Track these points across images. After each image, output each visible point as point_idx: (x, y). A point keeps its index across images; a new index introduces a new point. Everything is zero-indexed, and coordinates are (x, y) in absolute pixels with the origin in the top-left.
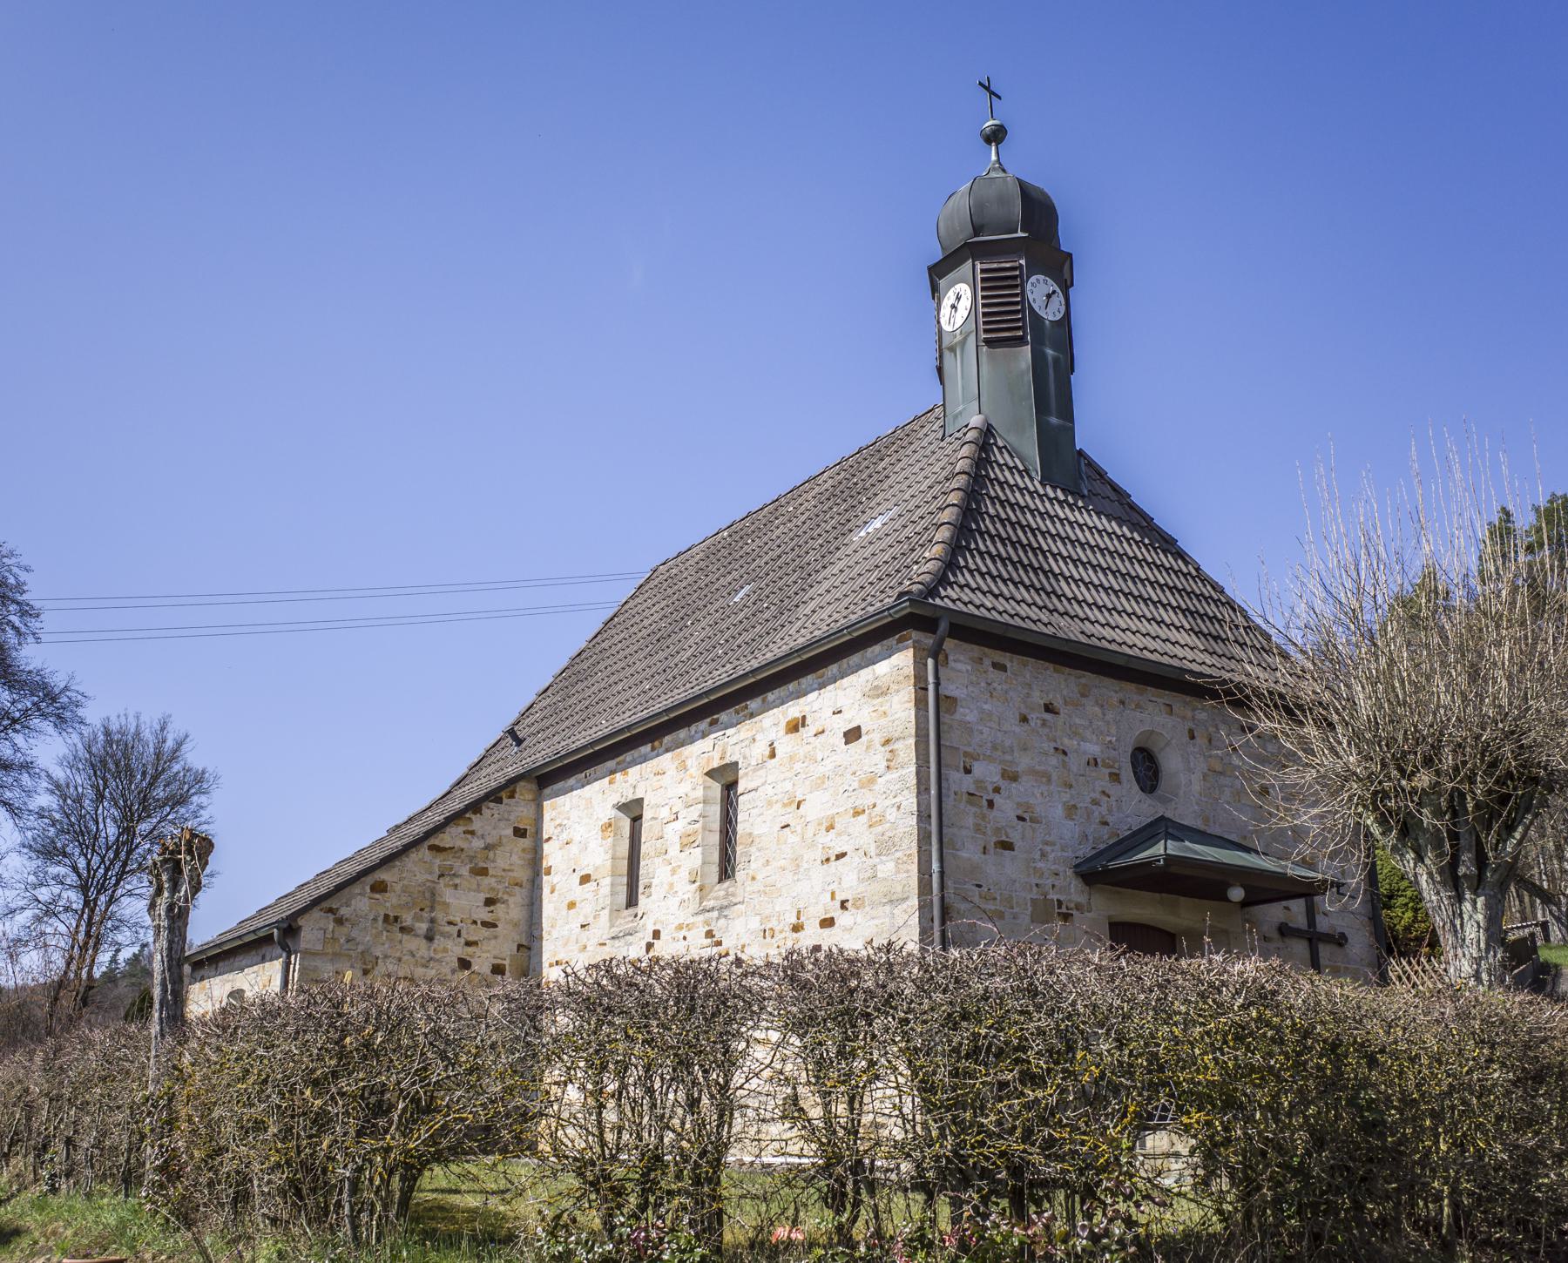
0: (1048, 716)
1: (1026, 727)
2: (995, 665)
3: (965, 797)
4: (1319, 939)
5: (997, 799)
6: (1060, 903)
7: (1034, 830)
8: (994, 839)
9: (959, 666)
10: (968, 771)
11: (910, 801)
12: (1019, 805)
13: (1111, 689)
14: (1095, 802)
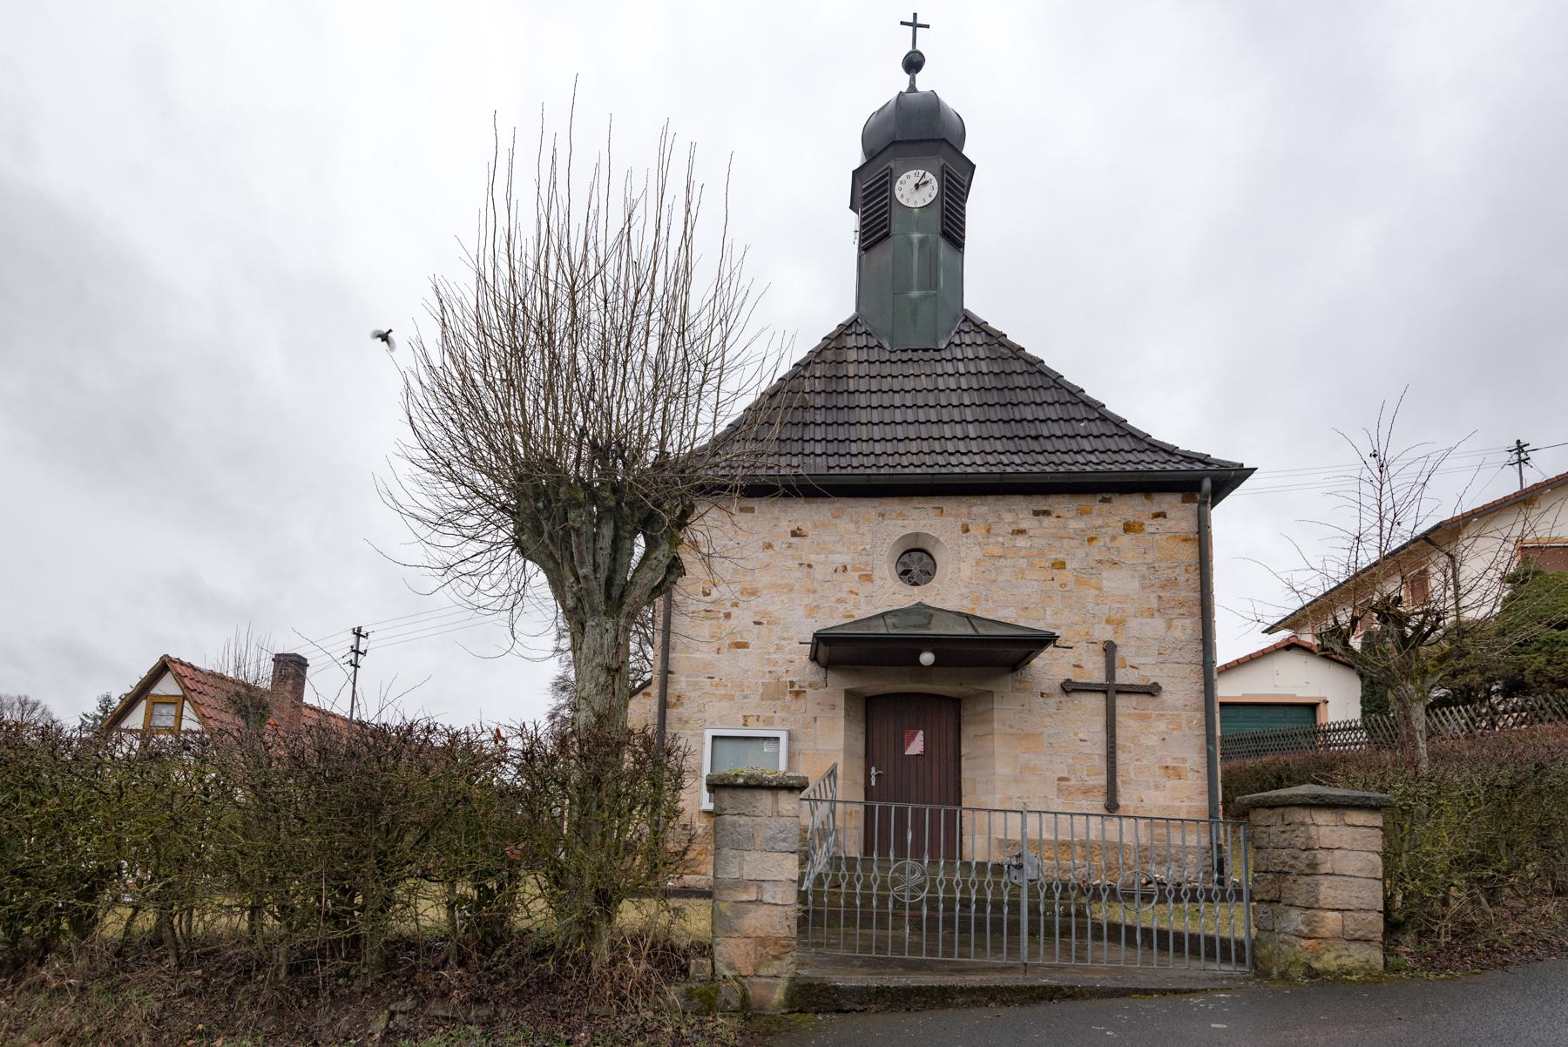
0: (795, 540)
1: (770, 552)
4: (1118, 692)
5: (734, 611)
6: (792, 684)
13: (867, 509)
14: (840, 601)
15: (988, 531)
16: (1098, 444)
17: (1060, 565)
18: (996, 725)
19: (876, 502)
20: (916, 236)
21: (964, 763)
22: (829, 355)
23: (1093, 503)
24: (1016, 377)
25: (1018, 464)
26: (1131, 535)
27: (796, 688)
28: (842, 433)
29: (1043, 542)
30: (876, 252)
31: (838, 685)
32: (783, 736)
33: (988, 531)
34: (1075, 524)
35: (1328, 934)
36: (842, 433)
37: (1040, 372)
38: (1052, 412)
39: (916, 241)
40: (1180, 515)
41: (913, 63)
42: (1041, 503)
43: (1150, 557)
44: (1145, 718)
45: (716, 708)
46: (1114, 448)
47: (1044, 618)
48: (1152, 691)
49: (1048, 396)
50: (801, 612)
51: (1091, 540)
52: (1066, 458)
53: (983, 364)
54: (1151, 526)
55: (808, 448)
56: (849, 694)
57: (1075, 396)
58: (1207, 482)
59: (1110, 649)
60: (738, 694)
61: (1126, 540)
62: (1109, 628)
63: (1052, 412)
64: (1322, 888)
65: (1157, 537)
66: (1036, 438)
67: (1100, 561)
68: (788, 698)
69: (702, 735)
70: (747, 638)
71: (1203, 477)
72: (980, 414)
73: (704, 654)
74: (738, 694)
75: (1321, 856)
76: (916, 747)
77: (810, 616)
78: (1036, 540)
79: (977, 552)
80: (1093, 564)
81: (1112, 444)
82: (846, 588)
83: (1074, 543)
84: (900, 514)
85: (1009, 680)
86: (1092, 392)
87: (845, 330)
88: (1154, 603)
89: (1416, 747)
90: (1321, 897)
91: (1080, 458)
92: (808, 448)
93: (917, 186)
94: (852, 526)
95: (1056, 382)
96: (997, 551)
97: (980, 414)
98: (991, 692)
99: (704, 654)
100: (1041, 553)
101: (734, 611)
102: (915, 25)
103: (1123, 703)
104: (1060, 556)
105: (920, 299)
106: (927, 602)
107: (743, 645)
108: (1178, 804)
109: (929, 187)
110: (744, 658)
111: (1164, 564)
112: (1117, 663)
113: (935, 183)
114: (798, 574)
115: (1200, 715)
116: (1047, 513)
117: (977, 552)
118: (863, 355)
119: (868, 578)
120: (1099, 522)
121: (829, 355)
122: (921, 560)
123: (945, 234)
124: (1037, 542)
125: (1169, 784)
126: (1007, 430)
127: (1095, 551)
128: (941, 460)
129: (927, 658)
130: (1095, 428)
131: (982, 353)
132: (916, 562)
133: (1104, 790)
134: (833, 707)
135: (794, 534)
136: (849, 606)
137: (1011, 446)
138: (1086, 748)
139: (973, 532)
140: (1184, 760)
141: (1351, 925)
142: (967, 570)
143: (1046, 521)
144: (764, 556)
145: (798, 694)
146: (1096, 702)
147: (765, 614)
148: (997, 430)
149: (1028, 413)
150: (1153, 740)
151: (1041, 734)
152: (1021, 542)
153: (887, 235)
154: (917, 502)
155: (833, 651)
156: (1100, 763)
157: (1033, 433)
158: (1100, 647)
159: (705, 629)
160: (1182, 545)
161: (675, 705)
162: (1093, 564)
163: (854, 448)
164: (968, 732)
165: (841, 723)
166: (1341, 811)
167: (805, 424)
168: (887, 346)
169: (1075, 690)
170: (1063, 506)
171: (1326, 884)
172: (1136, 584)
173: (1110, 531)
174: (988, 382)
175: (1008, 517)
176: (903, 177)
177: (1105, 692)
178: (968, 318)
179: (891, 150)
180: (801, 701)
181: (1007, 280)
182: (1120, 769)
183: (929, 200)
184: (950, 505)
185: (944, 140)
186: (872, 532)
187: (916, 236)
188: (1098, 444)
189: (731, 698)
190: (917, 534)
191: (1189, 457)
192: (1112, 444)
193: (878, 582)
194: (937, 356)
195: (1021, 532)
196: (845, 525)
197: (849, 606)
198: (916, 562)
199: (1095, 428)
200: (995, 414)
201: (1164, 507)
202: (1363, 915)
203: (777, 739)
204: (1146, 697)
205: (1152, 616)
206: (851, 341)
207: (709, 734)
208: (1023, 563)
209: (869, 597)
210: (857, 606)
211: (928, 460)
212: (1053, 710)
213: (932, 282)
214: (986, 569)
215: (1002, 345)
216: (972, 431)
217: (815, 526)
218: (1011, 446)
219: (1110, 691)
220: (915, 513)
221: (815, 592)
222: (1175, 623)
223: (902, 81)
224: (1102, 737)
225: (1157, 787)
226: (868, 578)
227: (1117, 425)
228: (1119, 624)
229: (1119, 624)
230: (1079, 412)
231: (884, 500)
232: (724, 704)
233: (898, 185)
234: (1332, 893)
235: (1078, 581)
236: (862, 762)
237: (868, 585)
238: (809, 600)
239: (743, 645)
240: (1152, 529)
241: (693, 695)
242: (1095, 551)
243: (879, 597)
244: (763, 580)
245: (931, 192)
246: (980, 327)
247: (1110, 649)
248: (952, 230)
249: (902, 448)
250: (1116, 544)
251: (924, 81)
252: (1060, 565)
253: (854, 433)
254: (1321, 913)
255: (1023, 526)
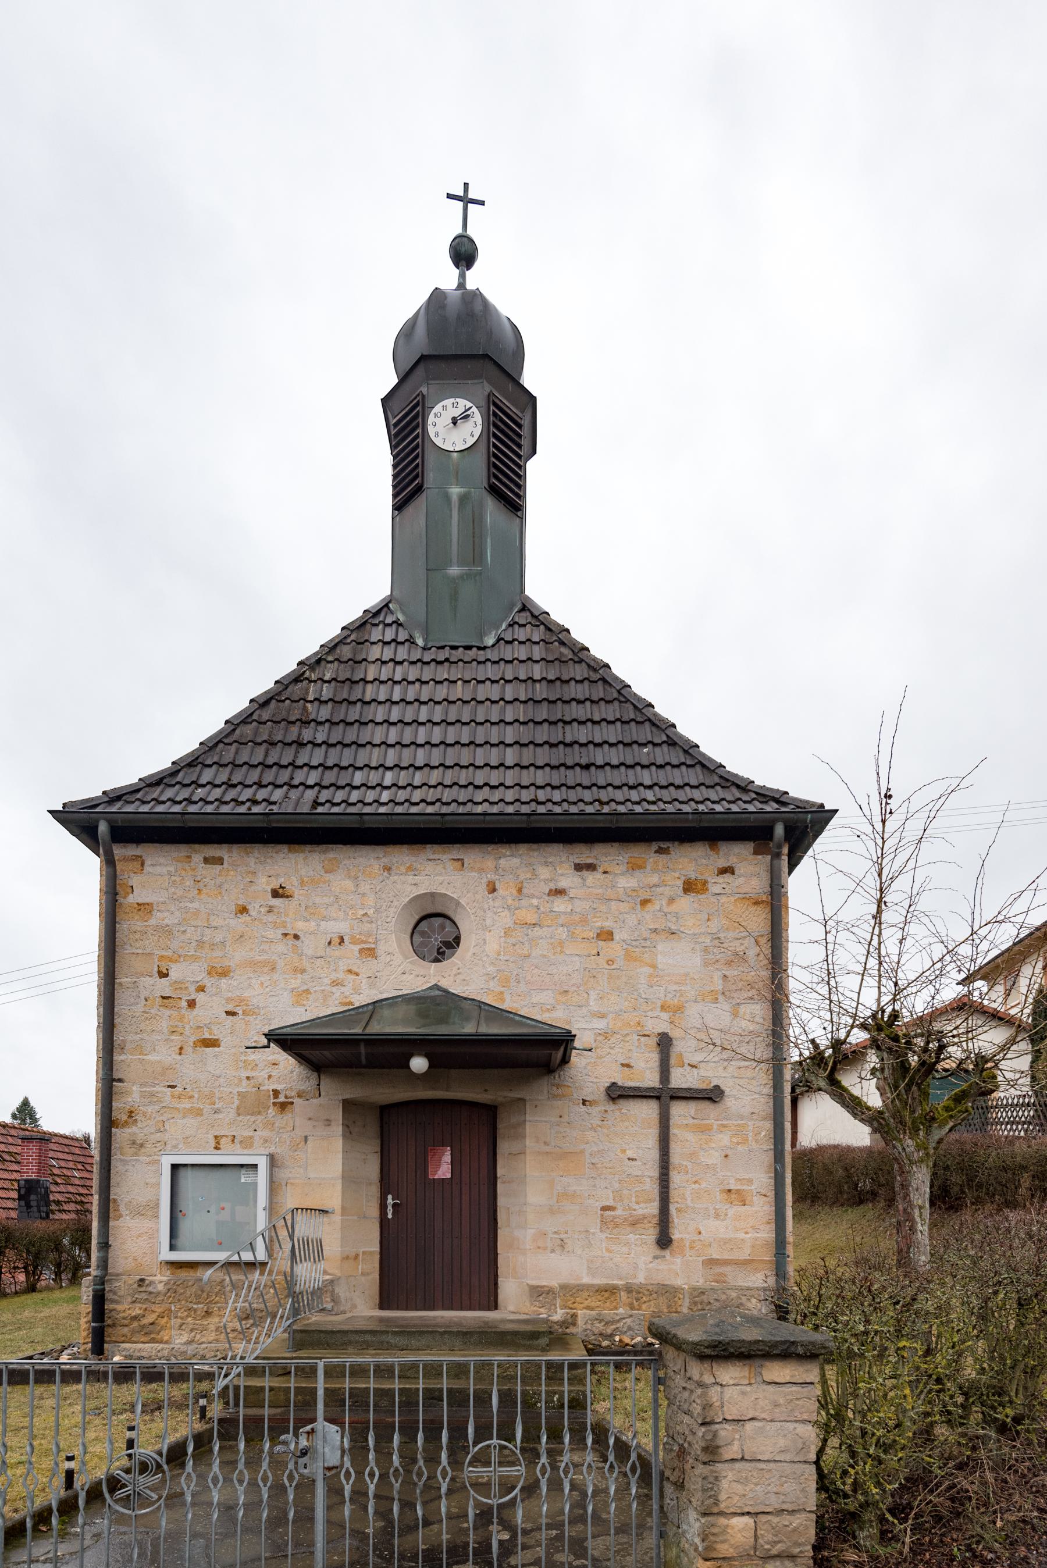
0: (277, 902)
1: (245, 918)
2: (206, 860)
3: (159, 1001)
4: (673, 1098)
5: (200, 998)
6: (276, 1093)
7: (247, 1023)
8: (193, 1039)
9: (158, 869)
10: (163, 975)
11: (684, 1086)
12: (229, 1000)
13: (368, 861)
14: (336, 983)
15: (520, 891)
16: (662, 777)
17: (606, 935)
18: (529, 1142)
19: (379, 851)
20: (455, 491)
21: (500, 1188)
22: (346, 652)
23: (645, 853)
24: (577, 687)
25: (585, 804)
26: (691, 897)
27: (282, 1099)
28: (347, 757)
29: (586, 905)
30: (410, 510)
31: (335, 1092)
32: (263, 1163)
33: (520, 891)
34: (626, 882)
35: (731, 1552)
36: (347, 757)
37: (604, 680)
38: (612, 734)
39: (455, 498)
40: (749, 867)
41: (464, 254)
42: (584, 854)
43: (714, 926)
44: (705, 1129)
45: (179, 1128)
46: (678, 782)
47: (587, 1004)
48: (712, 1096)
49: (611, 712)
50: (286, 998)
51: (645, 902)
52: (619, 795)
53: (537, 667)
54: (717, 884)
55: (299, 777)
56: (348, 1106)
57: (642, 713)
58: (787, 829)
59: (664, 1043)
60: (207, 1109)
61: (686, 903)
62: (665, 1016)
63: (612, 734)
64: (724, 1484)
65: (723, 899)
66: (587, 767)
67: (655, 931)
68: (272, 1111)
69: (157, 1162)
70: (217, 1033)
71: (774, 822)
72: (525, 734)
73: (162, 1055)
74: (207, 1109)
75: (725, 1432)
76: (444, 1171)
77: (298, 1003)
78: (577, 903)
79: (506, 919)
80: (646, 934)
81: (677, 776)
82: (343, 966)
83: (624, 907)
84: (410, 868)
85: (542, 1087)
86: (663, 709)
87: (372, 617)
88: (719, 985)
89: (913, 1229)
90: (723, 1497)
91: (634, 795)
92: (299, 777)
93: (454, 421)
94: (349, 884)
95: (621, 693)
96: (531, 918)
97: (525, 734)
98: (523, 1100)
99: (162, 1055)
100: (584, 920)
101: (200, 998)
102: (466, 200)
103: (679, 1111)
104: (608, 924)
105: (461, 577)
106: (444, 983)
107: (212, 1043)
108: (742, 1235)
109: (471, 421)
110: (214, 1061)
111: (731, 934)
112: (673, 1061)
113: (477, 417)
114: (281, 948)
115: (769, 1125)
116: (591, 867)
117: (506, 919)
118: (388, 653)
119: (370, 952)
120: (655, 879)
121: (346, 652)
122: (442, 927)
123: (494, 490)
124: (580, 906)
125: (732, 1211)
126: (558, 756)
127: (648, 917)
128: (463, 795)
129: (419, 1064)
130: (662, 755)
131: (537, 652)
132: (435, 931)
133: (655, 1220)
134: (328, 1122)
135: (275, 894)
136: (347, 990)
137: (556, 778)
138: (635, 1168)
139: (501, 892)
140: (750, 1181)
141: (766, 1536)
142: (493, 943)
143: (591, 877)
144: (239, 923)
145: (283, 1106)
146: (649, 1110)
147: (241, 1001)
148: (543, 756)
149: (582, 734)
150: (714, 1158)
151: (583, 1151)
152: (560, 905)
153: (419, 489)
154: (431, 851)
155: (317, 1050)
156: (652, 1188)
157: (584, 761)
158: (653, 1041)
159: (165, 1019)
160: (753, 909)
161: (126, 1124)
162: (646, 934)
163: (358, 778)
164: (504, 1147)
165: (338, 1143)
166: (758, 1362)
167: (302, 745)
168: (420, 642)
169: (621, 1097)
170: (611, 858)
171: (730, 1476)
172: (697, 960)
173: (667, 891)
174: (541, 691)
175: (544, 873)
176: (438, 408)
177: (658, 1098)
178: (527, 607)
179: (420, 371)
180: (288, 1116)
181: (585, 560)
182: (674, 1194)
183: (471, 441)
184: (473, 855)
185: (486, 356)
186: (373, 890)
187: (455, 491)
188: (662, 777)
189: (199, 1113)
190: (433, 895)
191: (764, 795)
192: (677, 776)
193: (384, 958)
194: (481, 656)
195: (559, 892)
196: (340, 883)
197: (347, 990)
198: (435, 931)
199: (662, 755)
200: (542, 734)
201: (732, 861)
202: (786, 1519)
203: (255, 1166)
204: (706, 1104)
205: (716, 1000)
206: (376, 634)
207: (167, 1161)
208: (562, 933)
209: (373, 978)
210: (356, 991)
211: (447, 795)
212: (596, 1122)
213: (475, 555)
214: (530, 940)
215: (562, 643)
216: (511, 756)
217: (302, 883)
218: (556, 778)
219: (665, 1096)
220: (430, 867)
221: (303, 971)
222: (742, 1009)
223: (447, 277)
224: (654, 1154)
225: (717, 1216)
226: (370, 952)
227: (686, 752)
228: (675, 1010)
229: (675, 1010)
230: (645, 733)
231: (390, 849)
232: (191, 1121)
233: (431, 419)
234: (739, 1488)
235: (629, 956)
236: (375, 1190)
237: (372, 962)
238: (296, 982)
239: (212, 1043)
240: (716, 889)
241: (150, 1109)
242: (649, 918)
243: (391, 975)
244: (237, 955)
245: (472, 430)
246: (540, 619)
247: (664, 1043)
248: (507, 491)
249: (418, 778)
250: (674, 908)
251: (475, 279)
252: (606, 935)
253: (363, 757)
254: (723, 1521)
255: (563, 884)
